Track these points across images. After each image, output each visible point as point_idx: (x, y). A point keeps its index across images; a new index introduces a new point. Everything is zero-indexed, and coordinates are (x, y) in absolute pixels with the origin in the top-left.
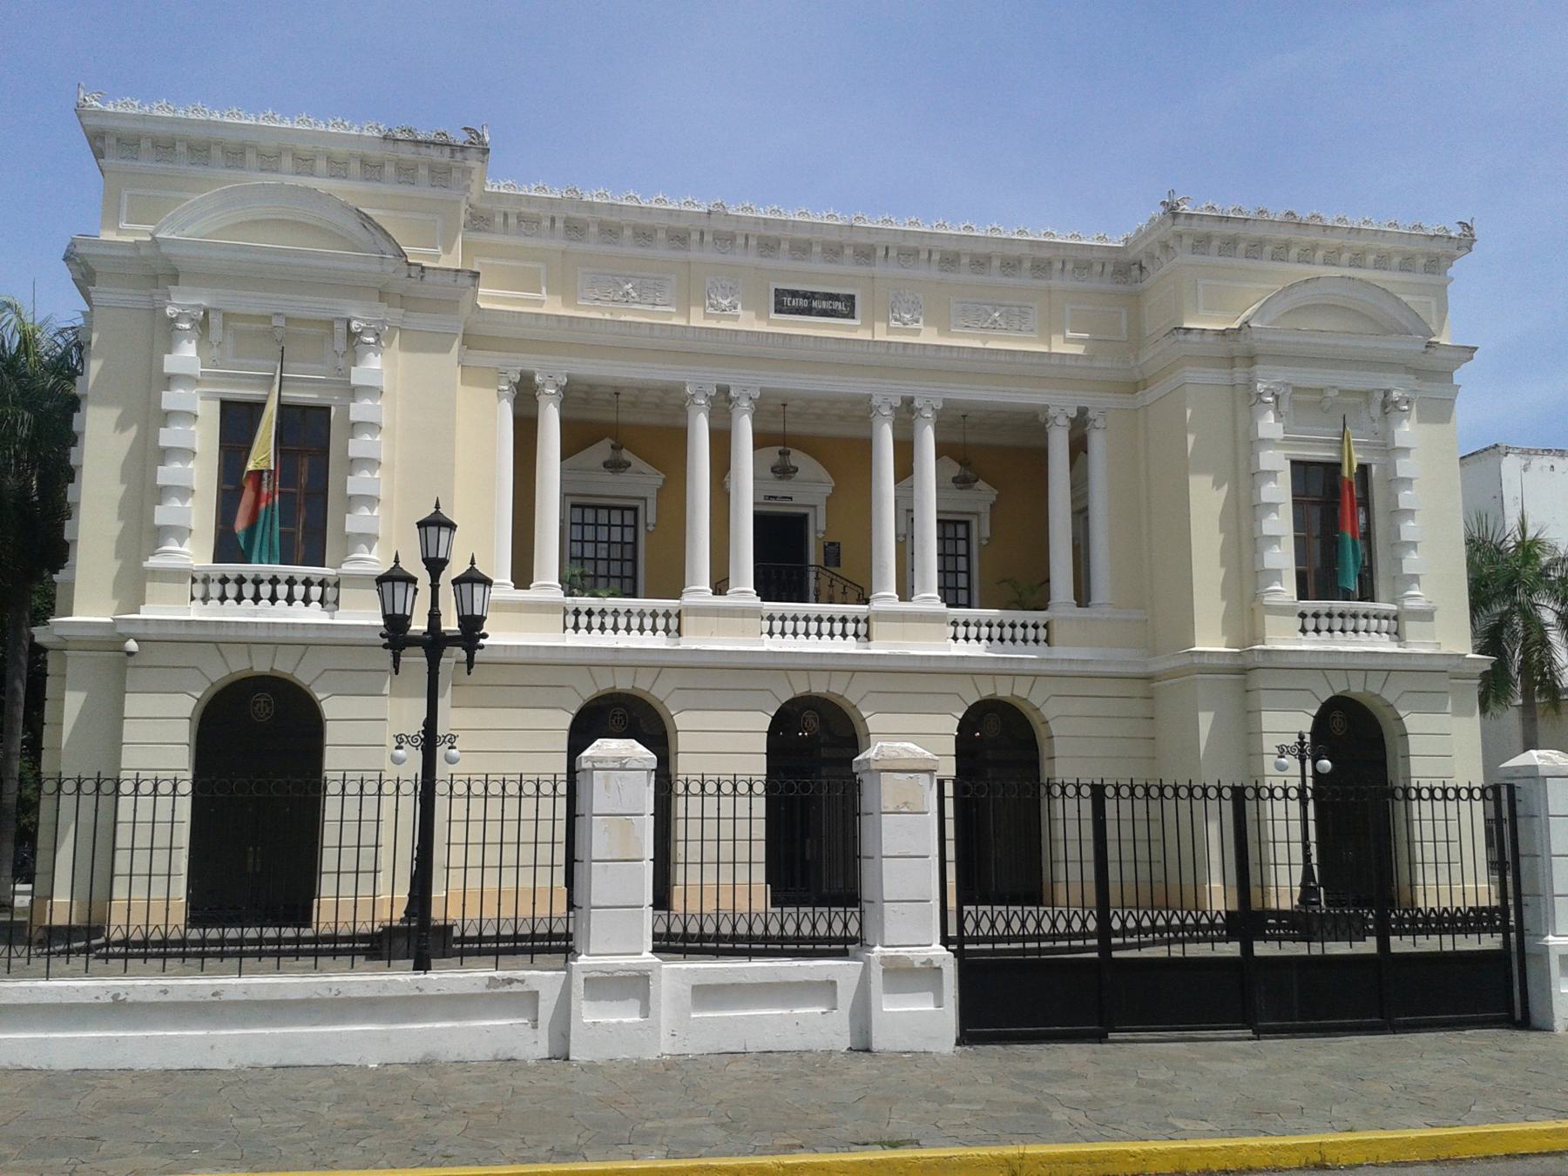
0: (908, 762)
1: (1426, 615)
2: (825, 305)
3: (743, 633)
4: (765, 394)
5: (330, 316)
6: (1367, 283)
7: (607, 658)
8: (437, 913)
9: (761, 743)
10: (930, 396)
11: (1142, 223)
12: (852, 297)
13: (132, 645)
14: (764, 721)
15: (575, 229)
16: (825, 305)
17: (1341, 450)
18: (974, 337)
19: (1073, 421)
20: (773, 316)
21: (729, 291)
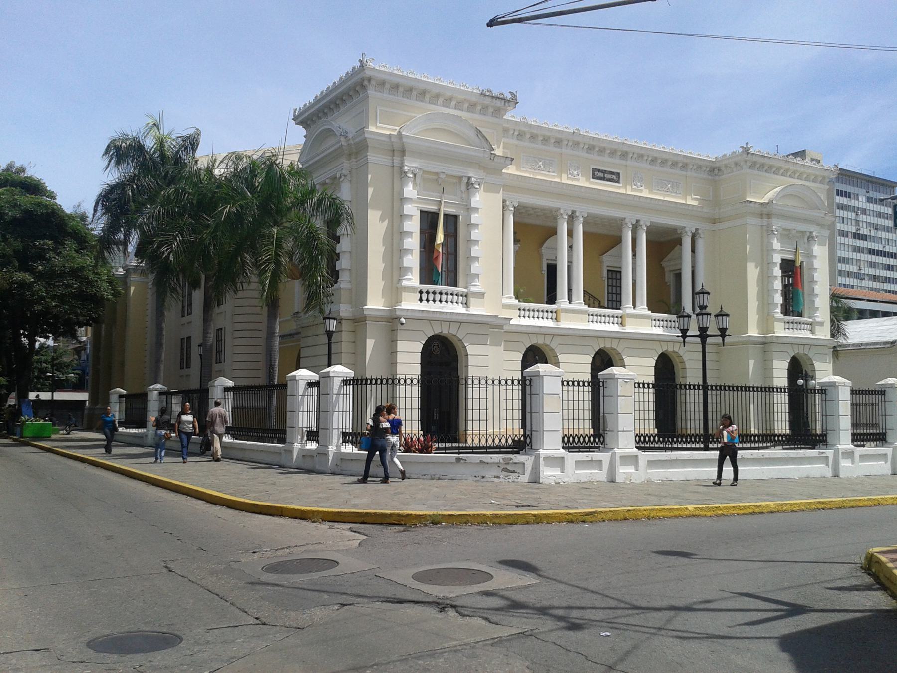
0: (635, 372)
1: (481, 295)
2: (609, 176)
3: (582, 320)
4: (589, 215)
5: (461, 174)
6: (808, 188)
7: (537, 330)
8: (710, 432)
9: (418, 358)
10: (647, 220)
11: (728, 152)
12: (619, 174)
13: (403, 320)
14: (419, 347)
15: (521, 135)
16: (609, 176)
17: (795, 255)
18: (661, 195)
19: (569, 216)
20: (592, 180)
21: (577, 168)
